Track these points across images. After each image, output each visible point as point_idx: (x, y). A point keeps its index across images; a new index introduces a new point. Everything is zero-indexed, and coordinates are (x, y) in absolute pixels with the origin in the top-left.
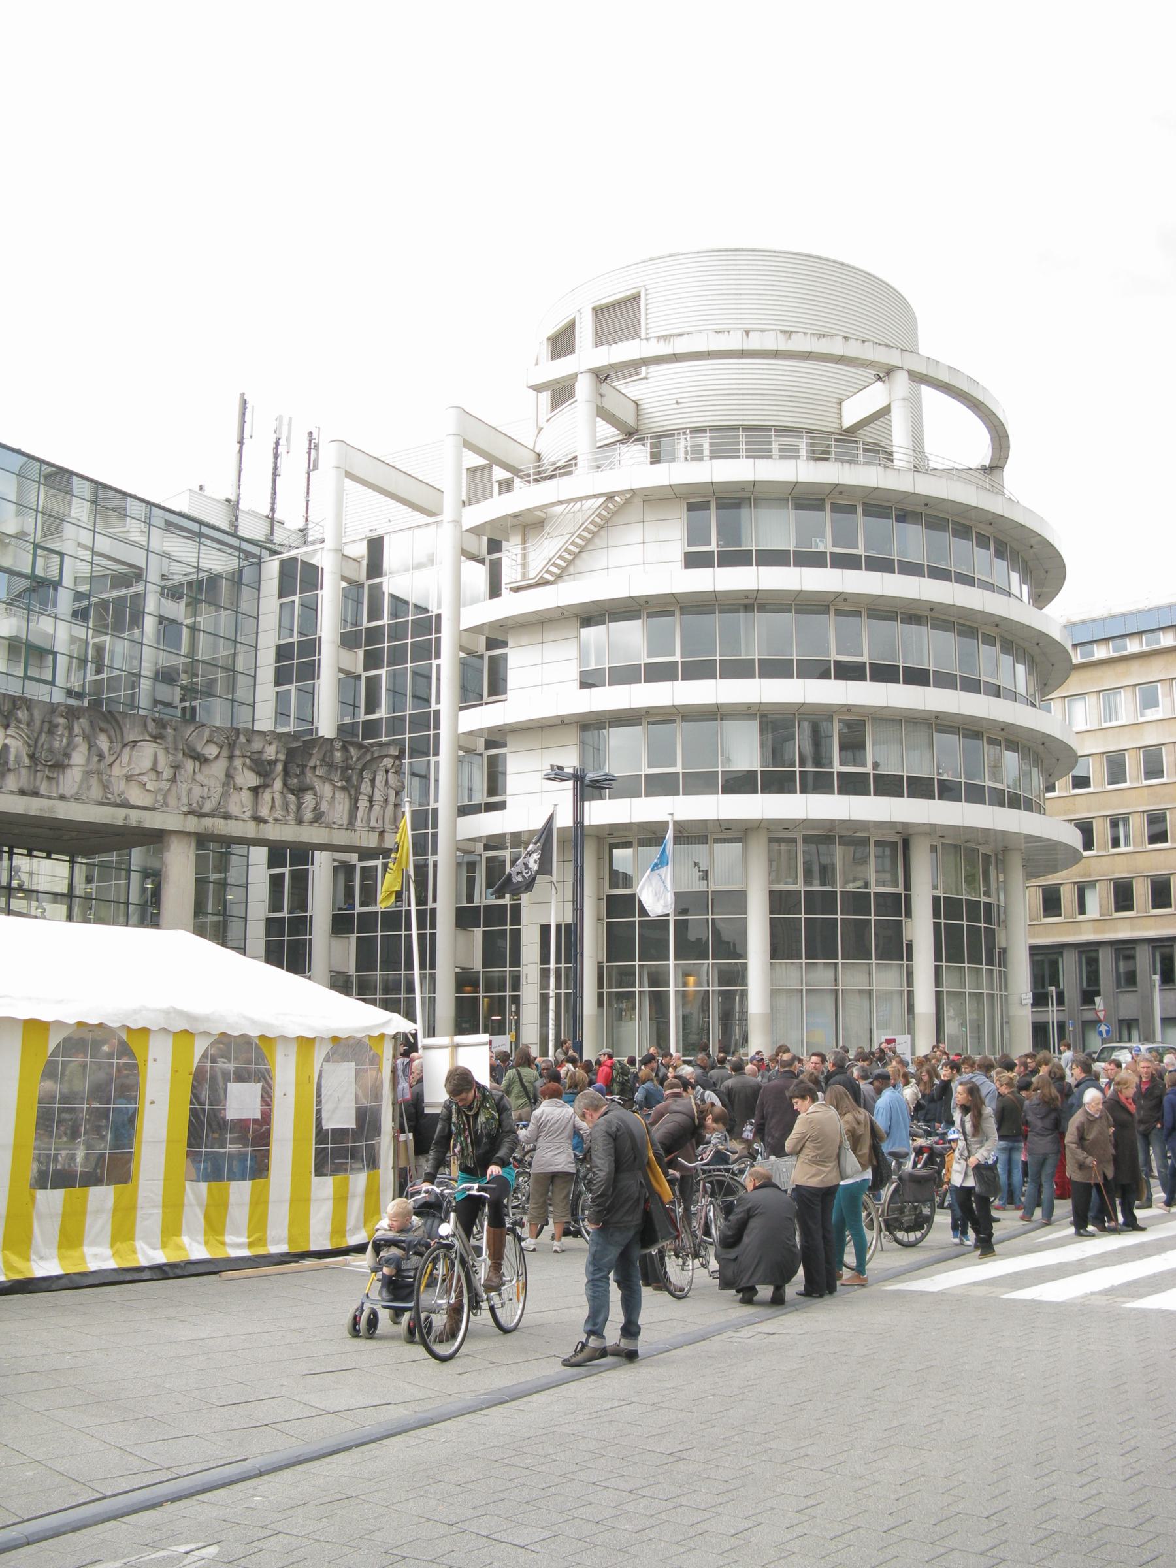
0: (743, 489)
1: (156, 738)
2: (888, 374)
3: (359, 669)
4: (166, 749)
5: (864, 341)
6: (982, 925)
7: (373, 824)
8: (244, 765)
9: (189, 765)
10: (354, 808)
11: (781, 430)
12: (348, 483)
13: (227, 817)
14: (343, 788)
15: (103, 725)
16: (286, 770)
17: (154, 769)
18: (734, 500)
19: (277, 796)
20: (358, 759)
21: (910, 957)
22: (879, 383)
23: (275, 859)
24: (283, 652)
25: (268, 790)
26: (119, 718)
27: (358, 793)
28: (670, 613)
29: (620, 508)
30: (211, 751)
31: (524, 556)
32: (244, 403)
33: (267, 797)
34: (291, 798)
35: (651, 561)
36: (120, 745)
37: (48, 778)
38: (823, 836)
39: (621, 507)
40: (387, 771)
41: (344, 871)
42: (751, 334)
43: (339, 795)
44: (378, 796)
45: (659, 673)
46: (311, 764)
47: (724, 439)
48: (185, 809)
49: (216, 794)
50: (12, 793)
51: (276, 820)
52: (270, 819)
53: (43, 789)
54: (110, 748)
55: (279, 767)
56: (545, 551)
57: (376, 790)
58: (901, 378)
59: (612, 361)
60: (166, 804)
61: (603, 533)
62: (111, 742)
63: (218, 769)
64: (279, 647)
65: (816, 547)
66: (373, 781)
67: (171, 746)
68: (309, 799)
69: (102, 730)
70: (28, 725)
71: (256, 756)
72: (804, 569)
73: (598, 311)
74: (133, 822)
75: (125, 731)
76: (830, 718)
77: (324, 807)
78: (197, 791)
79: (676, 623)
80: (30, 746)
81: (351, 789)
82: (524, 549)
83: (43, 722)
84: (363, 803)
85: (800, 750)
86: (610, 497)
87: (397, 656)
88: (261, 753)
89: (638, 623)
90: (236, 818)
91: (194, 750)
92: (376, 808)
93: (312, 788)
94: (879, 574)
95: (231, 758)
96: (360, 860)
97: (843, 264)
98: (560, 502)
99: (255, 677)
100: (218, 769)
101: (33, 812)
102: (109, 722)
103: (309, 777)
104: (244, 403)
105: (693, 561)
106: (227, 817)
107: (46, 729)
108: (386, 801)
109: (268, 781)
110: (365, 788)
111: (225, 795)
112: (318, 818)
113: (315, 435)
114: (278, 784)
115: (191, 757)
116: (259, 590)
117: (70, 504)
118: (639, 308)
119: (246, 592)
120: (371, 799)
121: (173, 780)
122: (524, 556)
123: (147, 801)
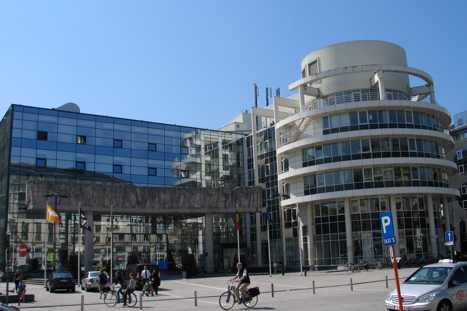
10: (249, 203)
13: (218, 208)
21: (428, 227)
30: (214, 193)
40: (257, 193)
50: (167, 208)
54: (189, 196)
55: (230, 195)
62: (190, 194)
80: (171, 198)
84: (251, 202)
92: (255, 202)
110: (252, 198)
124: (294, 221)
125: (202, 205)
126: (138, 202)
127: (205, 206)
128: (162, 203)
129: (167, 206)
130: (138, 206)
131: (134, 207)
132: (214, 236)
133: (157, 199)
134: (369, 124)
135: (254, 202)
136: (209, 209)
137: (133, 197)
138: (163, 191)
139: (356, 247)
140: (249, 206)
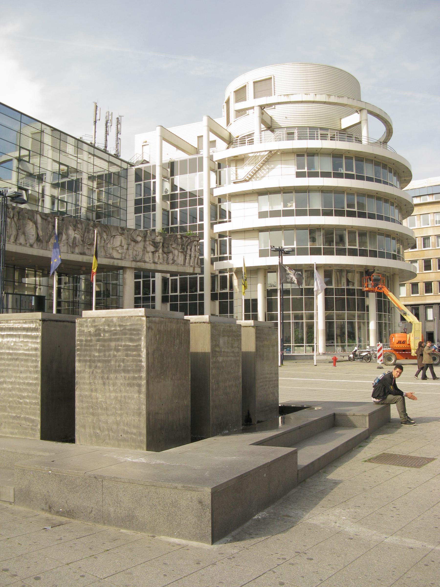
0: (317, 150)
1: (122, 234)
2: (360, 111)
3: (168, 208)
4: (125, 238)
5: (354, 99)
6: (383, 299)
7: (191, 264)
8: (150, 244)
9: (133, 243)
10: (185, 259)
11: (321, 129)
12: (164, 142)
13: (145, 262)
14: (181, 252)
15: (105, 230)
16: (163, 245)
17: (121, 245)
18: (312, 153)
19: (160, 255)
20: (186, 242)
21: (368, 311)
22: (357, 114)
23: (137, 276)
24: (137, 202)
25: (157, 253)
26: (110, 227)
27: (187, 254)
28: (292, 192)
29: (273, 156)
30: (139, 239)
31: (236, 171)
32: (97, 107)
33: (157, 255)
34: (165, 255)
35: (284, 175)
36: (110, 237)
37: (88, 248)
38: (343, 270)
39: (273, 155)
40: (195, 246)
41: (165, 281)
42: (317, 95)
43: (180, 254)
44: (193, 255)
45: (287, 213)
46: (171, 243)
47: (310, 132)
48: (132, 259)
49: (141, 254)
50: (78, 254)
51: (161, 263)
52: (159, 263)
53: (87, 251)
54: (107, 238)
55: (161, 244)
56: (244, 171)
57: (192, 253)
58: (365, 112)
59: (267, 103)
60: (125, 258)
61: (267, 163)
62: (107, 236)
63: (141, 245)
64: (136, 200)
65: (340, 171)
66: (191, 249)
67: (126, 237)
68: (171, 256)
69: (105, 231)
70: (82, 230)
71: (153, 241)
72: (324, 178)
73: (254, 83)
74: (116, 264)
75: (112, 232)
76: (345, 230)
77: (175, 258)
78: (135, 252)
79: (293, 195)
80: (82, 237)
81: (184, 252)
82: (236, 169)
83: (86, 228)
84: (188, 257)
85: (333, 240)
86: (271, 151)
87: (184, 204)
88: (154, 239)
89: (280, 195)
90: (148, 263)
91: (134, 239)
92: (192, 259)
93: (172, 252)
94: (350, 180)
95: (145, 241)
96: (171, 276)
97: (341, 70)
98: (252, 153)
99: (126, 210)
100: (141, 245)
101: (85, 261)
102: (106, 228)
103: (171, 248)
104: (97, 107)
105: (299, 175)
106: (145, 262)
107: (87, 231)
108: (195, 256)
109: (158, 249)
110: (189, 252)
111: (143, 254)
112: (174, 261)
113: (120, 119)
114: (161, 251)
115: (133, 241)
116: (127, 179)
117: (66, 146)
118: (271, 83)
119: (122, 180)
120: (190, 255)
121: (128, 249)
122: (236, 171)
123: (119, 256)
124: (226, 274)
125: (123, 255)
126: (38, 239)
127: (127, 257)
128: (71, 244)
129: (77, 250)
130: (37, 244)
131: (31, 246)
132: (66, 168)
133: (64, 237)
134: (357, 211)
135: (190, 258)
136: (133, 262)
137: (31, 229)
138: (73, 225)
139: (228, 196)
140: (184, 264)
